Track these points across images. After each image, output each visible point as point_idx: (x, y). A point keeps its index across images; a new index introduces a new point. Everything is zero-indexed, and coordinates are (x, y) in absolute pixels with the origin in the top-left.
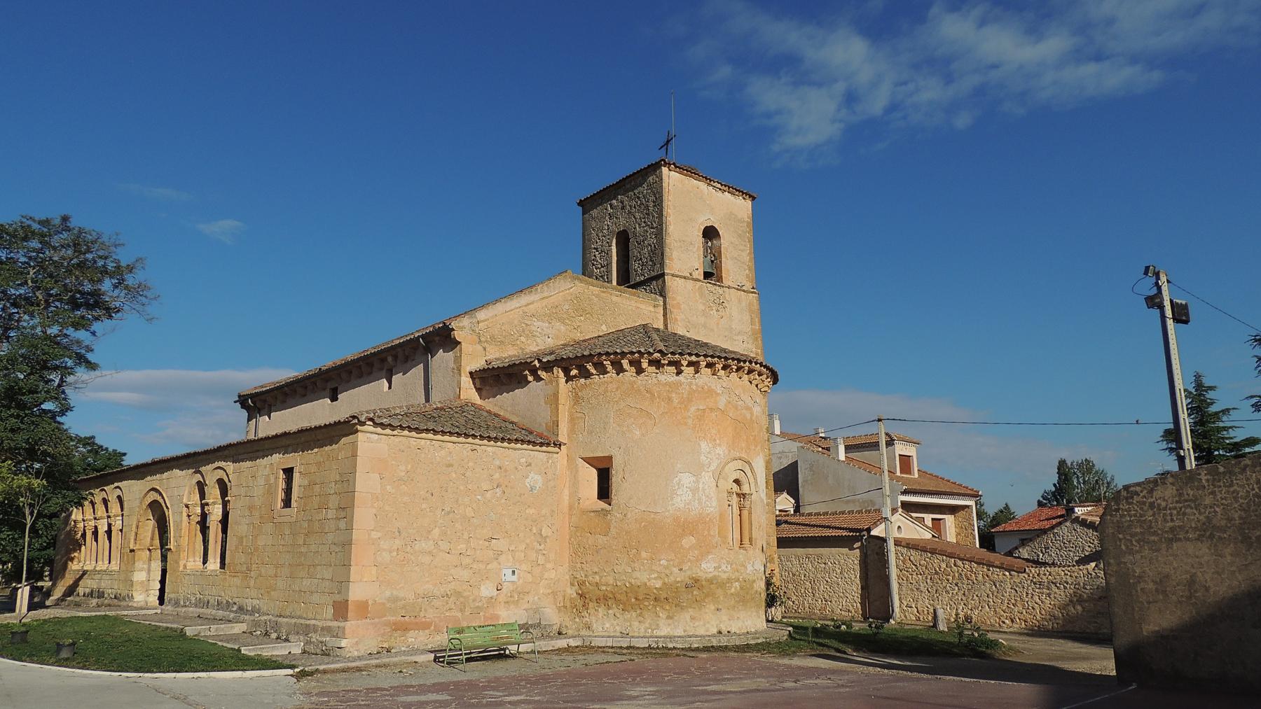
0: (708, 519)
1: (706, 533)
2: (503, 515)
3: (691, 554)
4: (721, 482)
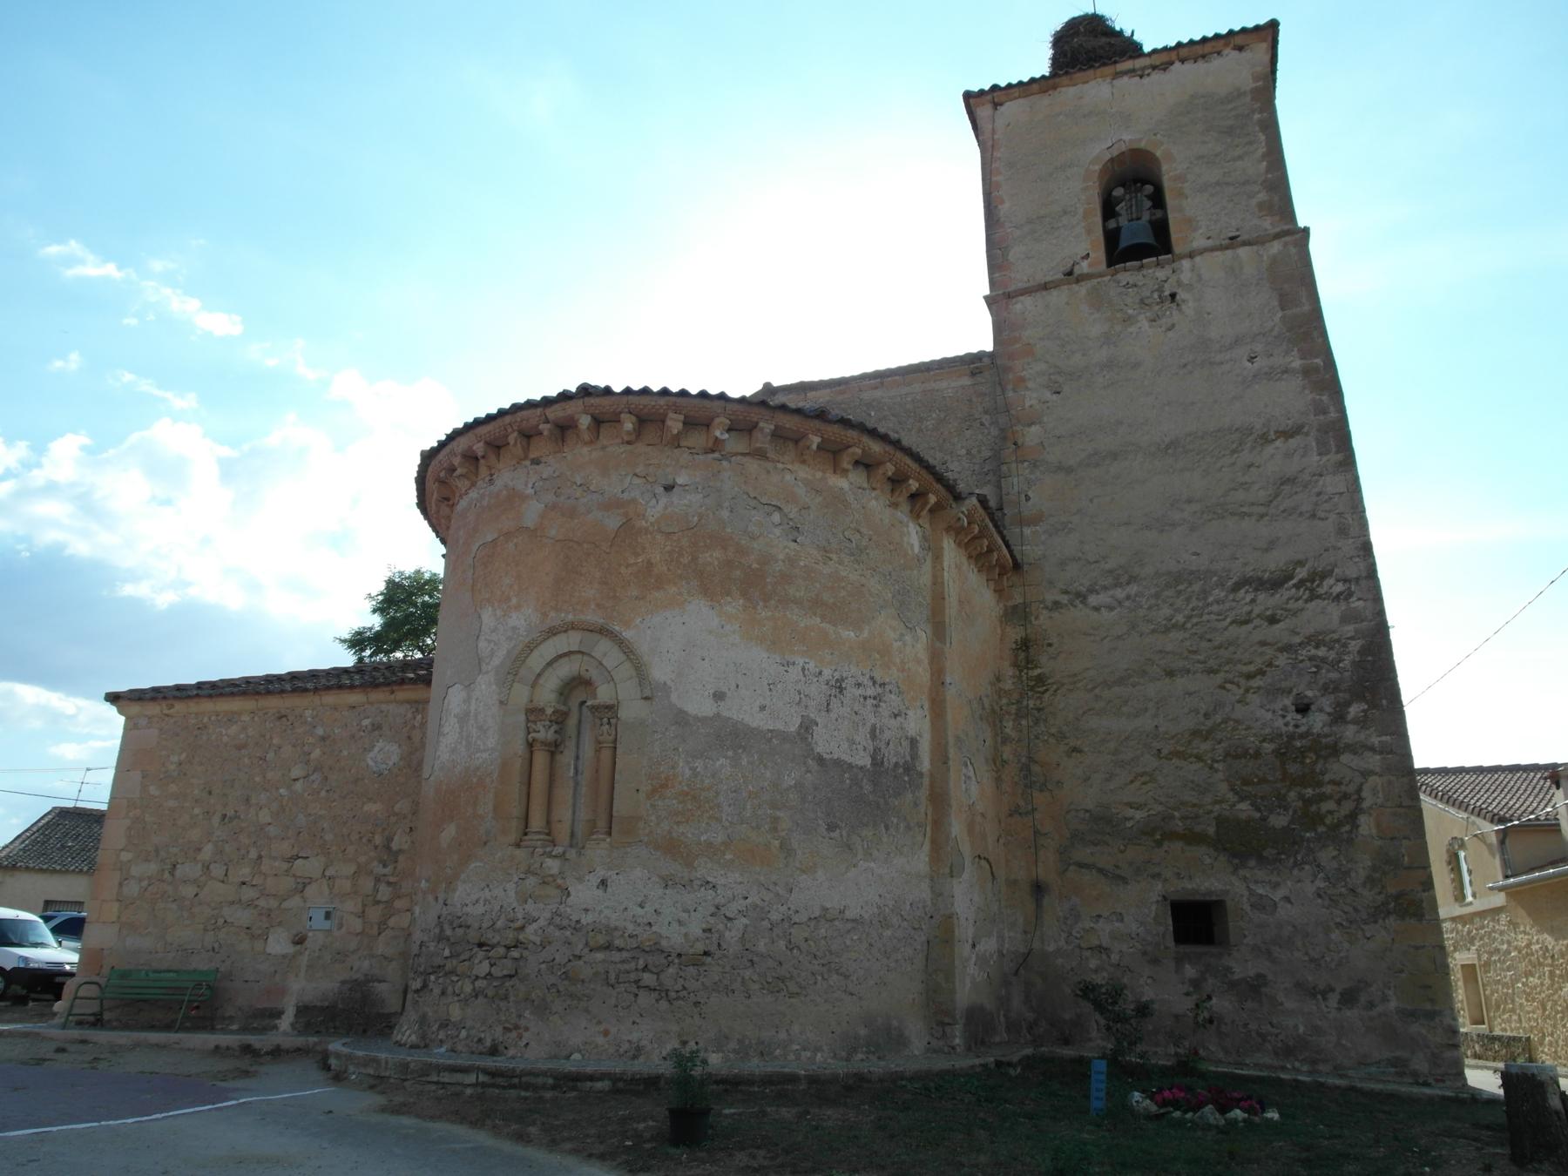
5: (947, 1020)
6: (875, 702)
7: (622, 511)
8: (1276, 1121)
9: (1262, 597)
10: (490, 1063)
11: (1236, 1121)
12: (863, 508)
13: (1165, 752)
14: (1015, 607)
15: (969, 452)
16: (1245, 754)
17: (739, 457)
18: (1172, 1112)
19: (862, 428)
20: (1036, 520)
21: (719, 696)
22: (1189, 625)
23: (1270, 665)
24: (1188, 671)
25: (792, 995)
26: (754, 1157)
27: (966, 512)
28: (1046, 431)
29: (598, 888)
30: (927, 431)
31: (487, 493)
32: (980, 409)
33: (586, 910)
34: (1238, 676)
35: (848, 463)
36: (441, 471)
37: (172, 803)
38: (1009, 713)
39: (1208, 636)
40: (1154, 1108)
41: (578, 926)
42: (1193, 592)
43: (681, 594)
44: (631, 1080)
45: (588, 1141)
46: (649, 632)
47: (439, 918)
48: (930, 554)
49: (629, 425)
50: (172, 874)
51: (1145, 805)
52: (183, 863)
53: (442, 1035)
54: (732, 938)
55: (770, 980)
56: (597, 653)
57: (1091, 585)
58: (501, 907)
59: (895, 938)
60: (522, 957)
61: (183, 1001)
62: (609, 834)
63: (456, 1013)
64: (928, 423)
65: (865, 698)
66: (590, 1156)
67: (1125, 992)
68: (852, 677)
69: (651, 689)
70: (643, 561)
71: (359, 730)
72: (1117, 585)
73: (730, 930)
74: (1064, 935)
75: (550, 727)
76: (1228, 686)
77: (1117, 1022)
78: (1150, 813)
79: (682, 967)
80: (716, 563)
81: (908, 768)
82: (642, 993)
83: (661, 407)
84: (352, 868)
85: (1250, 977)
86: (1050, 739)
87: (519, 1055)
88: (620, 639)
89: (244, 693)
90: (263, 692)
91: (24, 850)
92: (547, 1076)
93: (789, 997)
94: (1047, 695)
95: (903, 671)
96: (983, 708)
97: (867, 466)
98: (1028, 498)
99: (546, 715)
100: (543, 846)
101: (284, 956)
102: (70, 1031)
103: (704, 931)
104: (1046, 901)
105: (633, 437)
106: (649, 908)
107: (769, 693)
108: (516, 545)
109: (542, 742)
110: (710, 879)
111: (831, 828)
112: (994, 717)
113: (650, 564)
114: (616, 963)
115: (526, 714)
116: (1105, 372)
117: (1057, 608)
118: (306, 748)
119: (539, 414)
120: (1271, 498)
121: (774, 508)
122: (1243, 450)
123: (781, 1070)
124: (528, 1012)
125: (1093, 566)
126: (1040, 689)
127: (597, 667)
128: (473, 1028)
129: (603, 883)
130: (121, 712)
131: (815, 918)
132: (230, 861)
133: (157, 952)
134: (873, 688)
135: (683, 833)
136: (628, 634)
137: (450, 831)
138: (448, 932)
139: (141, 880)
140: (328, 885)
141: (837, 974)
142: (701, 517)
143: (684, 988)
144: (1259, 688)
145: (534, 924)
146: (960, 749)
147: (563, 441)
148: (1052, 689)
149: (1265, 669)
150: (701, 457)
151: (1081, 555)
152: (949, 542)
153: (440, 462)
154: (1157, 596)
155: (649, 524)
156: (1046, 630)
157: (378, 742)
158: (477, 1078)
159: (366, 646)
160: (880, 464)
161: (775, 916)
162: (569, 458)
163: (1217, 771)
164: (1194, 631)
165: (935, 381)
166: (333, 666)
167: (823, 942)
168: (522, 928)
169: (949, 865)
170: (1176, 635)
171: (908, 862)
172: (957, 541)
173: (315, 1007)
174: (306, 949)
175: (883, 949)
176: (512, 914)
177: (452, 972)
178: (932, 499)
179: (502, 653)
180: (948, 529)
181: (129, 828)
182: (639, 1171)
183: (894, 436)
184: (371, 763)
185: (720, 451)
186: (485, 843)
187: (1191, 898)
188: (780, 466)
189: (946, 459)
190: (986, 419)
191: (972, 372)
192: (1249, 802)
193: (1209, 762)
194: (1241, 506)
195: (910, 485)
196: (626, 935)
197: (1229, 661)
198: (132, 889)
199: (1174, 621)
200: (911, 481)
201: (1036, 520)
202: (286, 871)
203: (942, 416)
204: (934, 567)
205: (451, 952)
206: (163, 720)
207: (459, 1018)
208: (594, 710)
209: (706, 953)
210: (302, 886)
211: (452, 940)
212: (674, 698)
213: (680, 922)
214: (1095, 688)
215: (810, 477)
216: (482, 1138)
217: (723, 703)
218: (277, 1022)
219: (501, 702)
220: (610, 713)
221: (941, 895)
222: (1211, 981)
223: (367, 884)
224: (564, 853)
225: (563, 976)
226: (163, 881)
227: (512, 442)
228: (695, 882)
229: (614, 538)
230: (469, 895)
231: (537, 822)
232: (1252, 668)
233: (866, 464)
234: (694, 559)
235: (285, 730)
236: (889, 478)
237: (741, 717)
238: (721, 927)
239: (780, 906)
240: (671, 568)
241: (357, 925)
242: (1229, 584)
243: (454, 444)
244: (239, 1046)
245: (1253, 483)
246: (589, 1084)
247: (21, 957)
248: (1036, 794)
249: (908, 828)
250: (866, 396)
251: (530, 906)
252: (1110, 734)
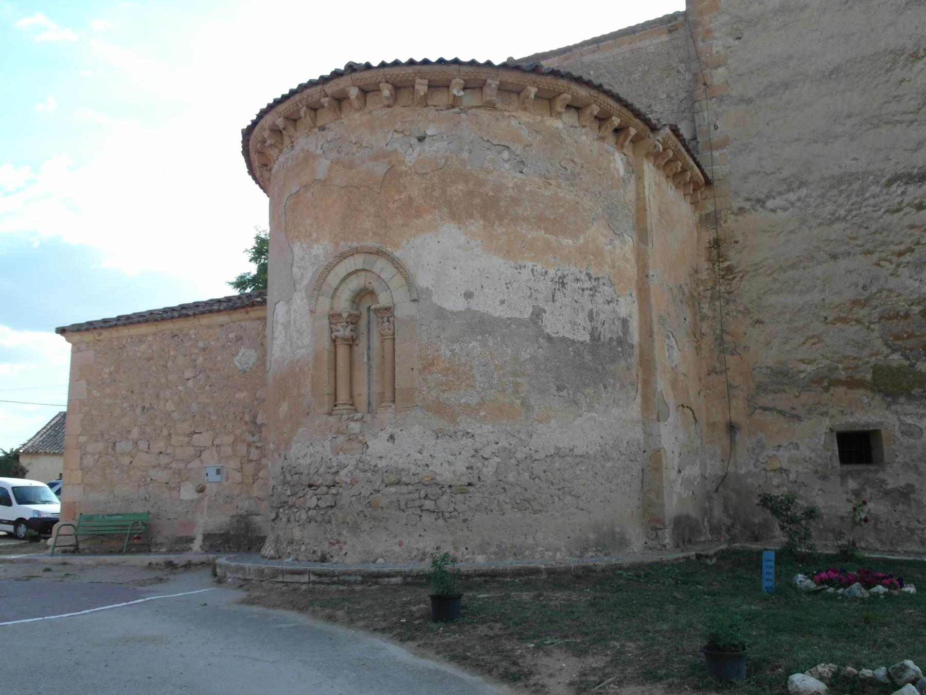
5: (658, 526)
6: (591, 293)
7: (387, 159)
8: (912, 594)
9: (911, 189)
10: (318, 567)
11: (878, 594)
12: (576, 142)
13: (830, 319)
14: (708, 215)
15: (668, 96)
16: (897, 316)
17: (474, 110)
18: (827, 589)
19: (569, 77)
20: (724, 144)
21: (469, 295)
22: (849, 217)
23: (918, 243)
24: (849, 254)
25: (535, 512)
26: (492, 628)
27: (661, 140)
28: (730, 71)
29: (388, 441)
30: (635, 82)
31: (290, 156)
32: (677, 59)
33: (381, 457)
34: (891, 255)
35: (561, 107)
36: (258, 143)
37: (108, 401)
38: (705, 297)
39: (865, 225)
40: (813, 586)
41: (376, 469)
42: (854, 190)
43: (435, 220)
44: (417, 576)
45: (376, 619)
46: (413, 250)
47: (282, 468)
48: (634, 176)
49: (386, 92)
50: (113, 448)
51: (815, 360)
52: (120, 442)
53: (289, 549)
54: (488, 472)
55: (519, 502)
56: (376, 270)
57: (768, 192)
58: (322, 458)
59: (616, 468)
60: (338, 493)
61: (126, 534)
62: (394, 401)
63: (297, 534)
64: (636, 76)
65: (583, 290)
66: (375, 630)
67: (796, 501)
68: (572, 274)
69: (417, 293)
70: (405, 197)
71: (228, 342)
72: (790, 190)
73: (487, 467)
74: (752, 461)
75: (346, 327)
76: (882, 263)
77: (790, 523)
78: (819, 365)
79: (453, 495)
80: (461, 194)
81: (620, 342)
82: (424, 514)
83: (410, 74)
84: (232, 438)
85: (901, 487)
86: (738, 315)
87: (341, 561)
88: (392, 257)
89: (147, 321)
90: (159, 319)
91: (42, 441)
92: (356, 575)
93: (534, 513)
94: (734, 282)
95: (614, 267)
96: (683, 294)
97: (578, 109)
98: (716, 127)
99: (343, 318)
100: (348, 414)
101: (192, 501)
102: (57, 557)
103: (467, 468)
104: (738, 437)
105: (391, 101)
106: (425, 453)
107: (506, 290)
108: (313, 194)
109: (342, 338)
110: (469, 431)
111: (560, 388)
112: (694, 301)
113: (410, 199)
114: (404, 494)
115: (329, 319)
116: (778, 17)
117: (741, 213)
118: (193, 357)
119: (319, 90)
120: (920, 106)
121: (504, 148)
122: (895, 68)
123: (527, 565)
124: (345, 531)
125: (769, 177)
126: (729, 277)
127: (377, 280)
128: (309, 544)
129: (392, 437)
130: (68, 340)
131: (551, 455)
132: (150, 438)
133: (109, 502)
134: (589, 282)
135: (447, 398)
136: (397, 254)
137: (284, 407)
138: (289, 478)
139: (94, 455)
140: (216, 450)
141: (570, 495)
142: (447, 159)
143: (455, 510)
144: (908, 263)
145: (345, 469)
146: (663, 325)
147: (340, 110)
148: (739, 276)
149: (913, 247)
150: (444, 112)
151: (759, 168)
152: (648, 165)
153: (256, 137)
154: (823, 196)
155: (408, 168)
156: (733, 231)
157: (241, 349)
158: (309, 578)
159: (247, 286)
160: (588, 105)
161: (520, 455)
162: (345, 123)
163: (873, 330)
164: (854, 221)
165: (640, 41)
166: (210, 299)
167: (558, 473)
168: (337, 472)
169: (656, 412)
170: (838, 226)
171: (624, 411)
172: (656, 165)
174: (206, 495)
175: (605, 476)
176: (330, 463)
177: (293, 506)
178: (633, 131)
179: (308, 275)
180: (648, 155)
181: (83, 420)
182: (407, 640)
183: (596, 82)
184: (237, 364)
185: (459, 106)
186: (308, 414)
187: (853, 429)
188: (507, 114)
189: (650, 102)
190: (682, 67)
191: (669, 30)
192: (899, 353)
193: (867, 324)
194: (894, 115)
195: (613, 121)
196: (411, 473)
197: (883, 243)
198: (89, 461)
199: (837, 215)
200: (614, 118)
201: (724, 144)
202: (188, 443)
203: (646, 68)
204: (637, 186)
205: (291, 492)
206: (96, 344)
207: (299, 538)
208: (376, 312)
209: (470, 484)
210: (199, 453)
211: (291, 484)
212: (435, 299)
213: (449, 463)
214: (772, 273)
215: (531, 121)
216: (303, 619)
217: (472, 300)
218: (191, 545)
219: (311, 311)
220: (388, 313)
221: (651, 435)
222: (869, 491)
223: (242, 449)
224: (362, 417)
225: (368, 505)
226: (108, 454)
227: (302, 114)
228: (458, 433)
229: (382, 181)
230: (299, 451)
231: (343, 396)
232: (902, 247)
233: (576, 107)
234: (444, 192)
235: (178, 346)
236: (596, 117)
237: (486, 310)
238: (480, 464)
239: (523, 448)
240: (426, 200)
241: (238, 477)
242: (883, 181)
243: (262, 122)
244: (164, 562)
245: (905, 95)
246: (386, 579)
247: (34, 511)
248: (728, 357)
249: (623, 386)
250: (587, 59)
251: (341, 457)
252: (785, 307)
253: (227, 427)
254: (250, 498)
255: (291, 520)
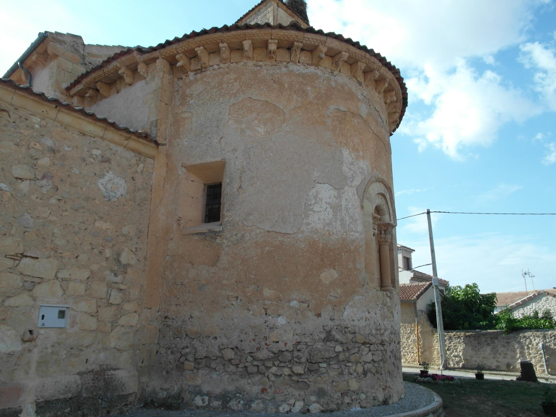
0: (352, 248)
1: (351, 265)
2: (51, 222)
3: (332, 294)
4: (366, 203)
63: (354, 385)
84: (85, 274)
101: (10, 355)
173: (58, 400)
184: (101, 187)
207: (357, 388)
223: (101, 289)
230: (355, 314)
241: (92, 323)
243: (329, 40)
253: (79, 258)
254: (105, 349)
255: (345, 373)
